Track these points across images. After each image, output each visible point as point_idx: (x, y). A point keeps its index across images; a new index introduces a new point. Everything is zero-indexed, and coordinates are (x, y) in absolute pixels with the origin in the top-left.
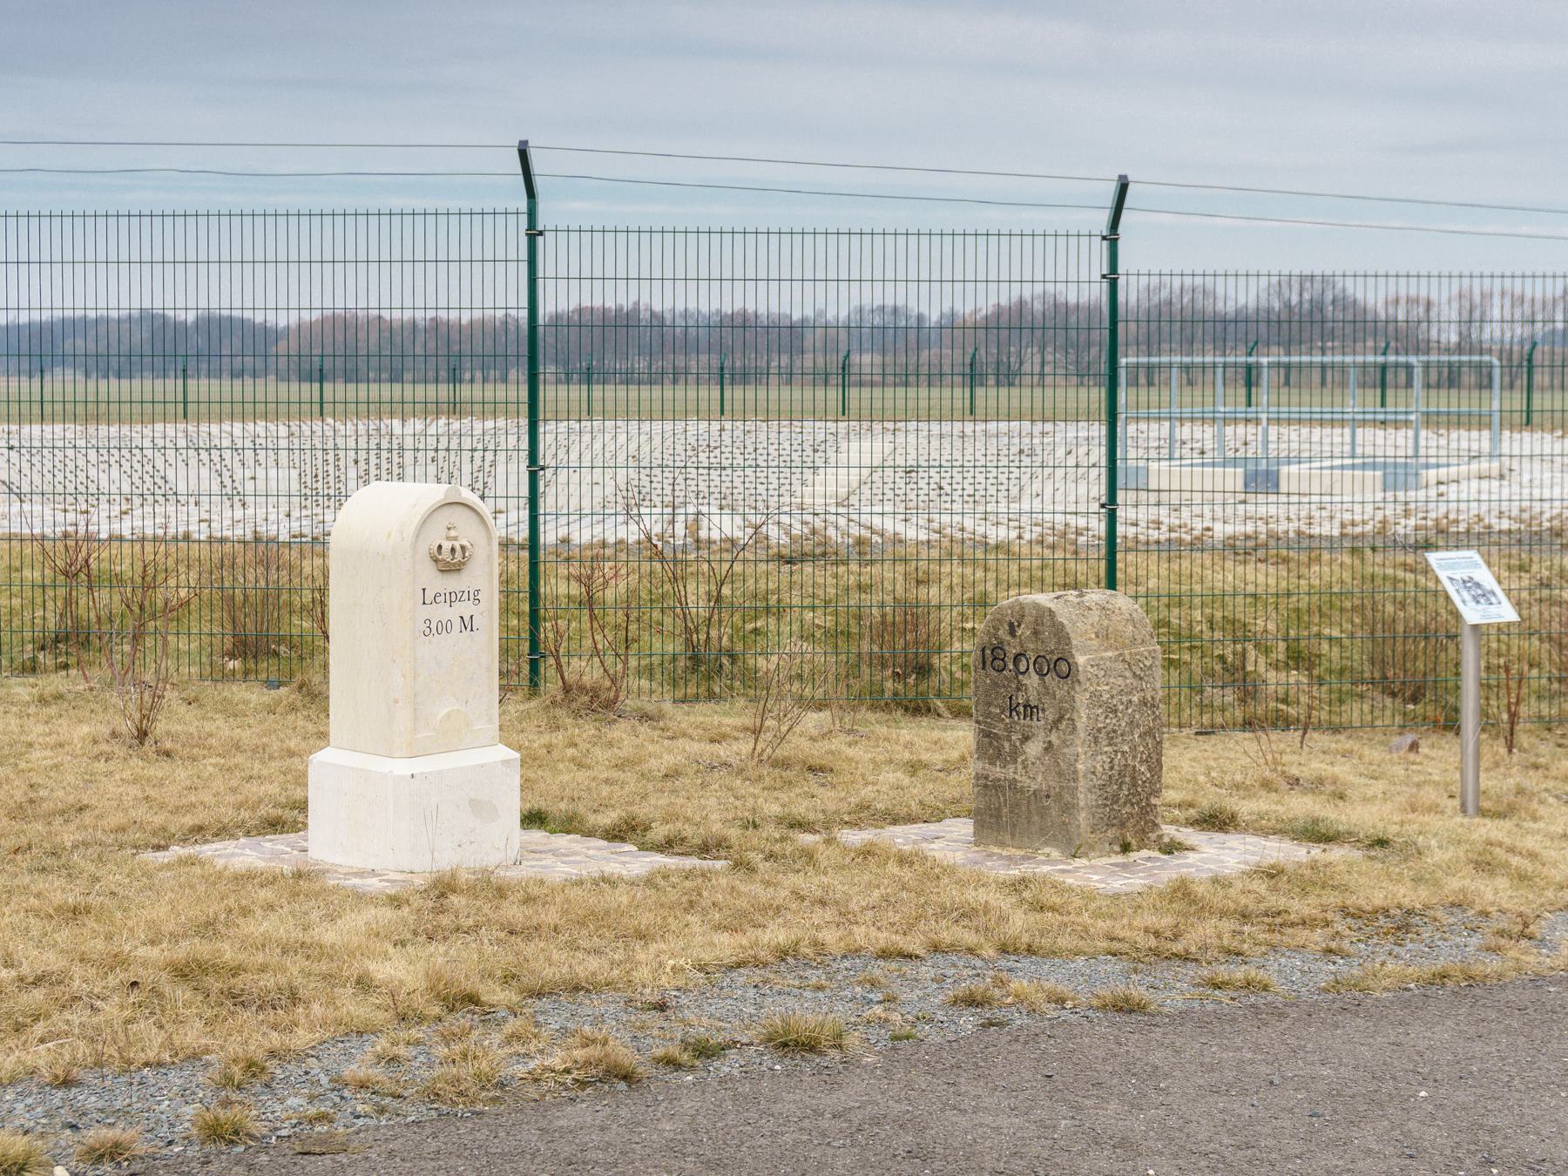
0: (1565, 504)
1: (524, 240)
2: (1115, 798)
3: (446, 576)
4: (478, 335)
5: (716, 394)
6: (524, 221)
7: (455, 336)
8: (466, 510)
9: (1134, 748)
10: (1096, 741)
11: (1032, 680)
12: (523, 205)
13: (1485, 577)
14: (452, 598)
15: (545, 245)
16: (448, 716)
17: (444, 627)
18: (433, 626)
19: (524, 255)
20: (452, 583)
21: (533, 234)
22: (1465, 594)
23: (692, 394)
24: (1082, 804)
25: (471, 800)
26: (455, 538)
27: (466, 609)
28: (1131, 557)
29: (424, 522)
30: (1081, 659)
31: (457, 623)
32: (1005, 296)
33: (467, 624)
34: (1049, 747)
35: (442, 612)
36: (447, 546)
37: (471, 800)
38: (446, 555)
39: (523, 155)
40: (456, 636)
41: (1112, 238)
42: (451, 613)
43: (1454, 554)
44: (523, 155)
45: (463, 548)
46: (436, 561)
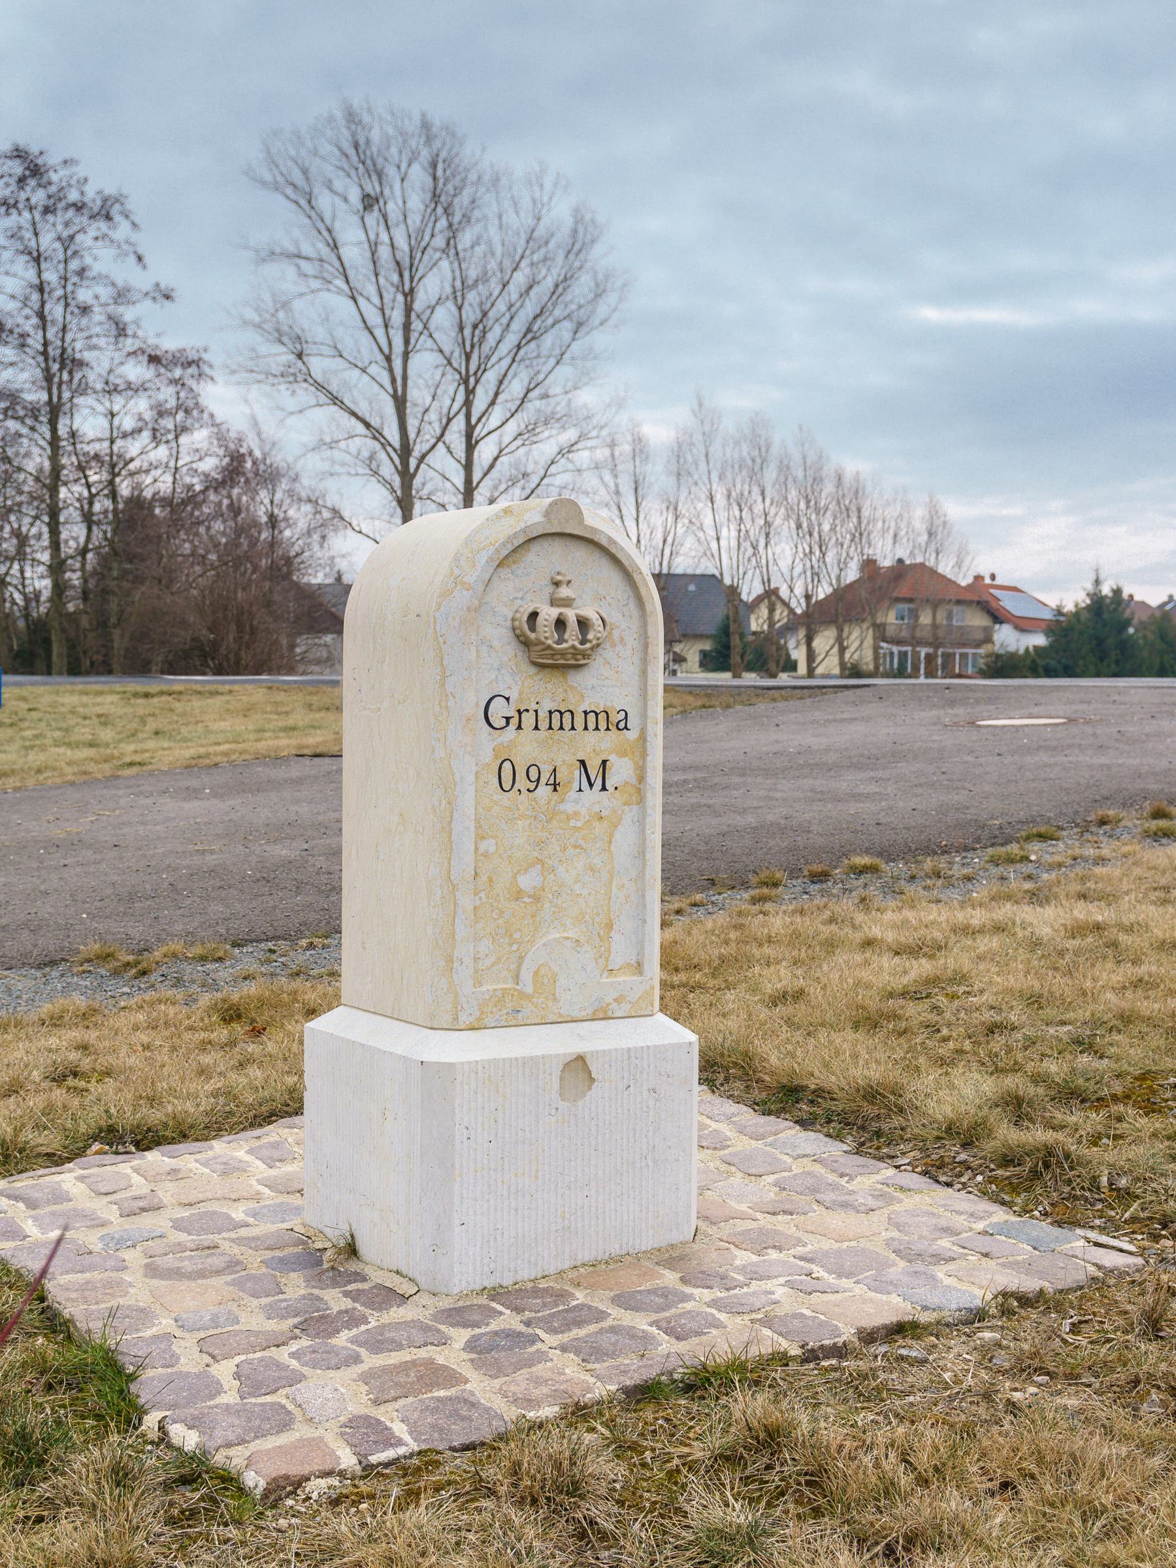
14: (560, 719)
31: (570, 775)
33: (594, 775)
45: (583, 624)
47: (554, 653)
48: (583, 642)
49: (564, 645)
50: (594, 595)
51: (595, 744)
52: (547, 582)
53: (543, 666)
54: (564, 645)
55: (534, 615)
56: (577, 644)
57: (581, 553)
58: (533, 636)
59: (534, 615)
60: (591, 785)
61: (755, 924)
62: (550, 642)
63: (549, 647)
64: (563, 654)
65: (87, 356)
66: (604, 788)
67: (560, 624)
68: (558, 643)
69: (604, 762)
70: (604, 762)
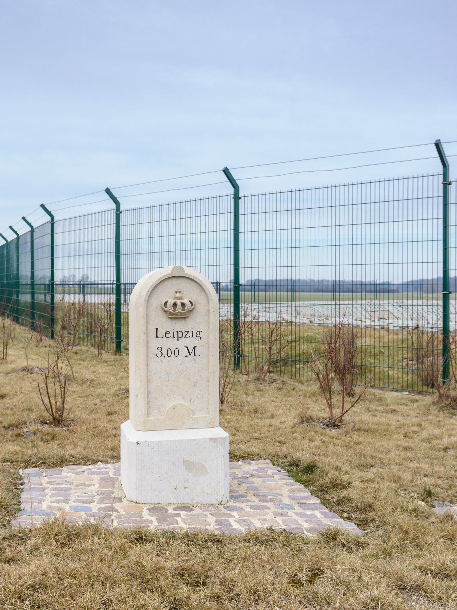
0: (456, 468)
1: (441, 186)
3: (174, 321)
6: (441, 178)
8: (190, 282)
12: (440, 169)
14: (179, 335)
16: (174, 407)
17: (175, 353)
18: (164, 352)
19: (441, 193)
20: (179, 326)
21: (446, 184)
25: (184, 462)
26: (180, 298)
27: (191, 342)
29: (156, 287)
31: (183, 351)
33: (191, 352)
37: (184, 462)
38: (170, 308)
39: (438, 145)
40: (182, 360)
42: (181, 344)
43: (168, 440)
44: (438, 145)
45: (183, 305)
46: (165, 311)
47: (174, 314)
48: (183, 310)
49: (177, 312)
50: (189, 294)
51: (191, 342)
52: (182, 291)
53: (171, 318)
54: (177, 312)
55: (166, 303)
56: (181, 311)
57: (184, 281)
58: (166, 309)
59: (166, 303)
60: (190, 354)
61: (424, 478)
62: (171, 311)
63: (171, 312)
64: (177, 314)
65: (315, 585)
66: (195, 355)
67: (175, 305)
68: (174, 311)
69: (195, 347)
70: (195, 347)
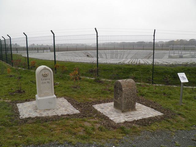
2: (128, 105)
4: (138, 43)
5: (134, 47)
7: (175, 42)
9: (131, 99)
10: (125, 99)
11: (119, 90)
13: (185, 76)
14: (46, 80)
15: (98, 37)
20: (46, 78)
22: (182, 78)
23: (131, 47)
24: (123, 106)
27: (48, 81)
28: (155, 59)
30: (123, 89)
32: (121, 42)
34: (120, 99)
35: (44, 81)
36: (44, 74)
41: (154, 36)
